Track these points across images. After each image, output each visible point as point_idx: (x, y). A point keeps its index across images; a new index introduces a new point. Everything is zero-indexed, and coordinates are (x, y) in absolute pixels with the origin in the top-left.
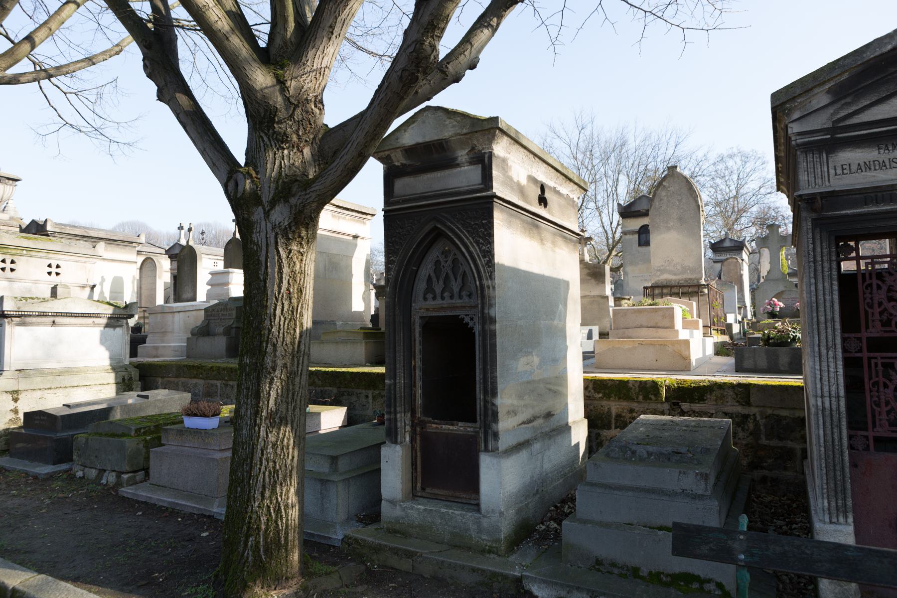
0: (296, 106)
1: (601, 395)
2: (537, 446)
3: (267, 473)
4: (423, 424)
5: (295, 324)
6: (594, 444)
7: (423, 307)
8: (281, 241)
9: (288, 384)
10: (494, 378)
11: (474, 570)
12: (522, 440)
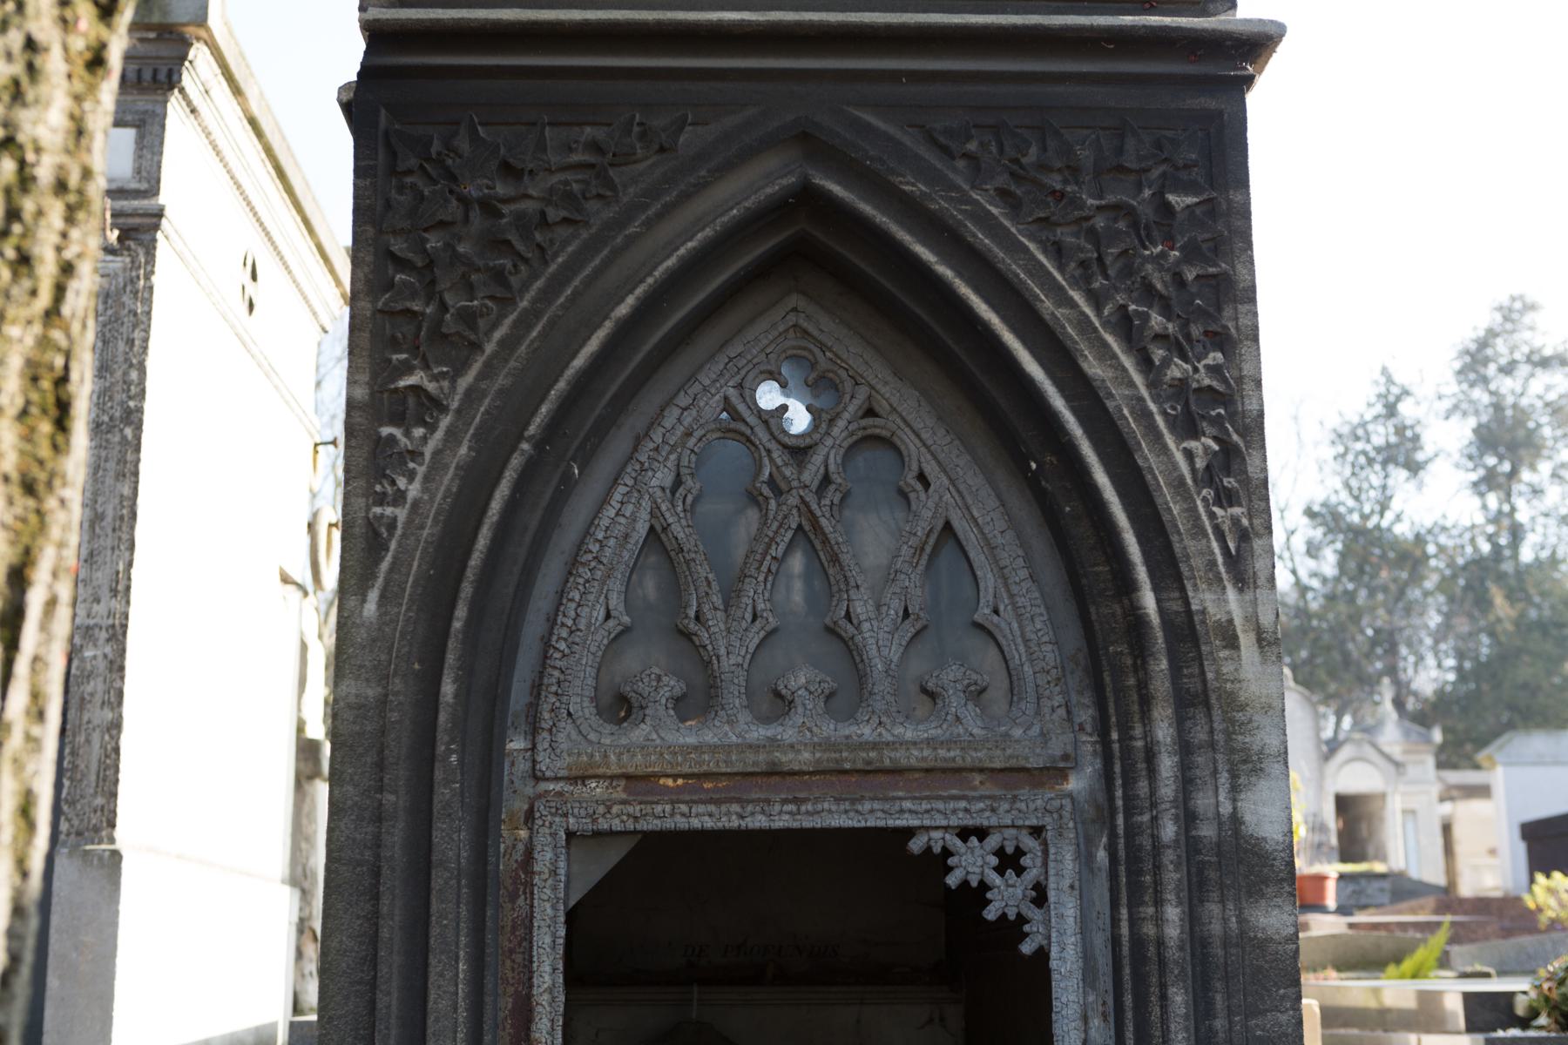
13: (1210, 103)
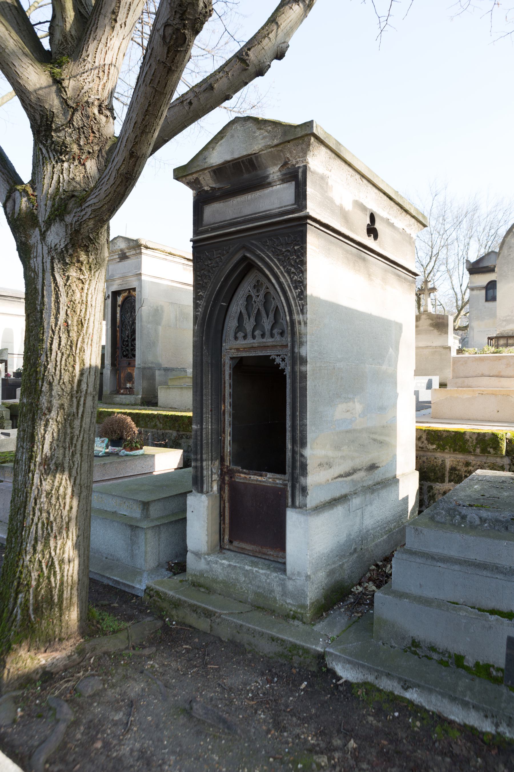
0: (75, 110)
1: (435, 446)
2: (356, 501)
3: (40, 525)
4: (231, 473)
5: (74, 361)
6: (426, 497)
7: (233, 347)
8: (58, 266)
9: (65, 427)
10: (304, 426)
11: (273, 639)
12: (337, 494)
13: (301, 229)
